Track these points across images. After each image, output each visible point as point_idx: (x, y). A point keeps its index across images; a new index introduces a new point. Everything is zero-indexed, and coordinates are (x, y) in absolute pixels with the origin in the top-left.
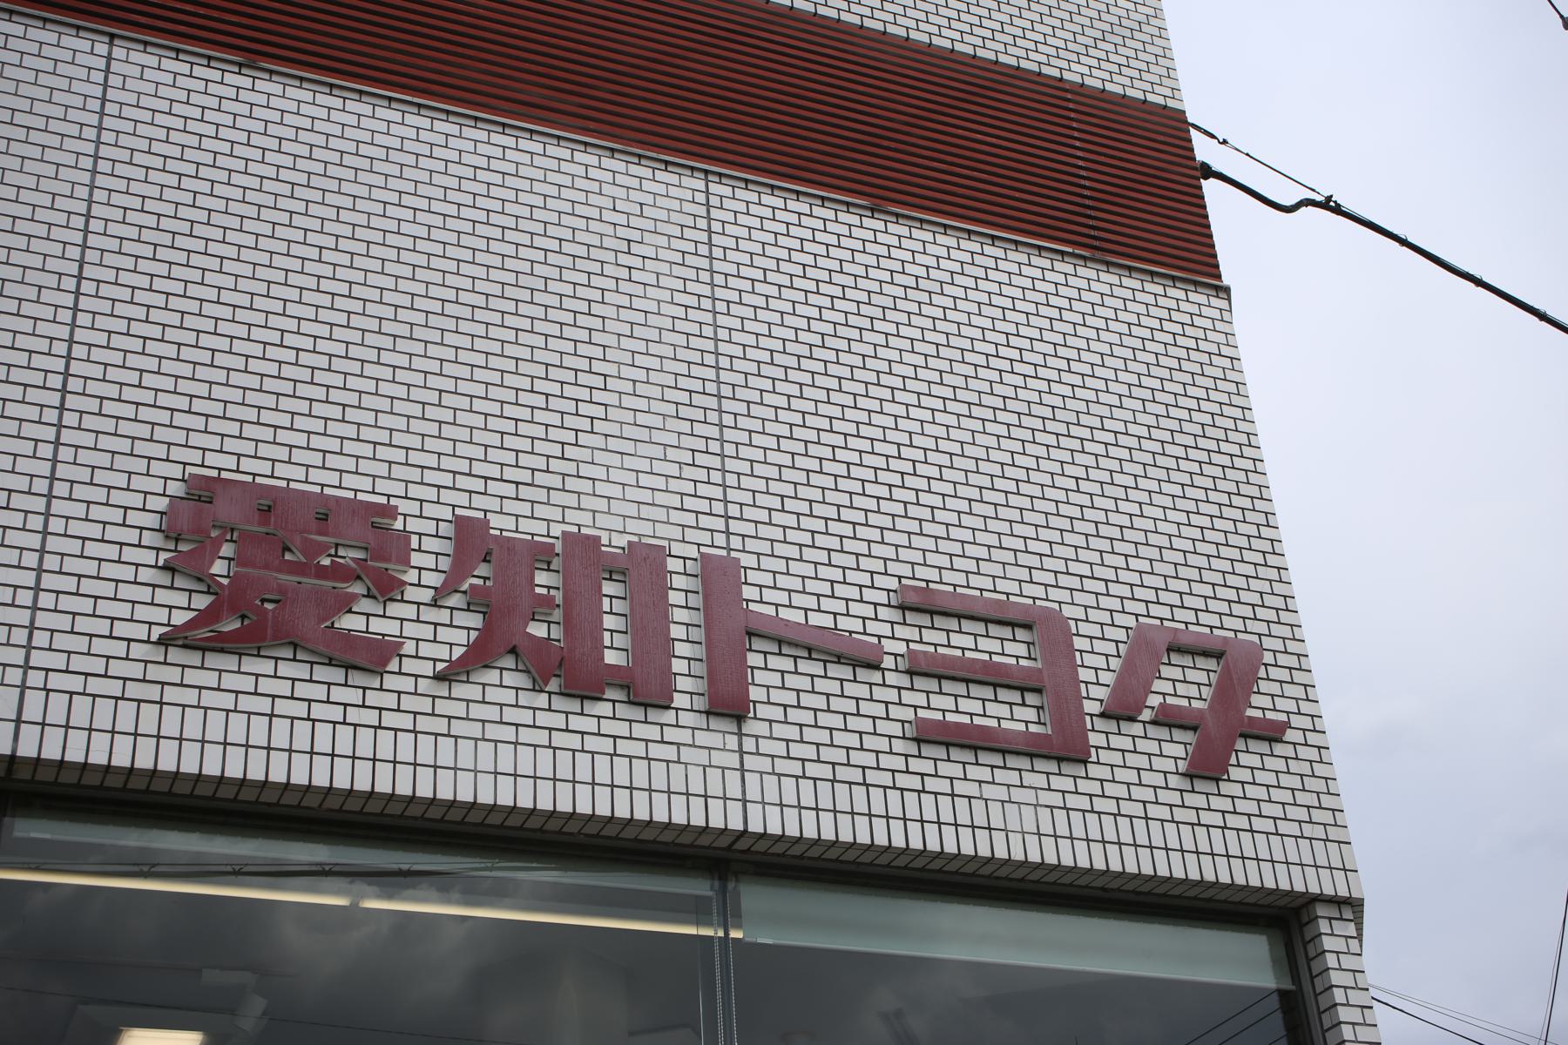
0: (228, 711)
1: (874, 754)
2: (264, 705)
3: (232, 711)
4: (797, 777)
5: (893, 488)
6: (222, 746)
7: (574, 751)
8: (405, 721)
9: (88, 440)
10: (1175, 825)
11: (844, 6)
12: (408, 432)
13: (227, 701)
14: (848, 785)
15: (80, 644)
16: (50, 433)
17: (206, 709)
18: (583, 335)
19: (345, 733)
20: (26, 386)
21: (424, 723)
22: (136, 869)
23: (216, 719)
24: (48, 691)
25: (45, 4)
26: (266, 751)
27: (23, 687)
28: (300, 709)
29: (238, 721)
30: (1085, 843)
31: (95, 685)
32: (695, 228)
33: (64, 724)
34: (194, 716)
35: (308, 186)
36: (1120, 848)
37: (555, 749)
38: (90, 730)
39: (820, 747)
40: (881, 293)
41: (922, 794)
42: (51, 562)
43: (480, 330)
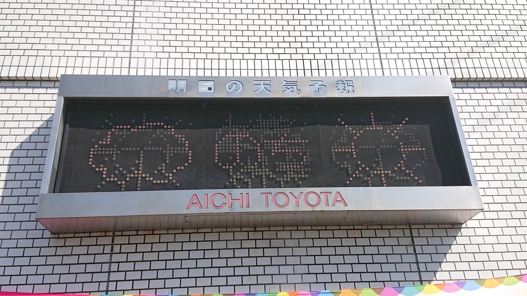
1: (444, 54)
3: (115, 57)
4: (446, 58)
5: (499, 42)
8: (264, 57)
9: (123, 19)
10: (423, 58)
11: (126, 3)
12: (329, 31)
13: (114, 54)
16: (131, 20)
17: (233, 59)
18: (425, 33)
20: (121, 17)
21: (185, 56)
22: (330, 212)
24: (268, 60)
26: (203, 70)
28: (191, 56)
29: (293, 63)
32: (485, 35)
33: (240, 69)
34: (230, 62)
37: (423, 59)
38: (204, 69)
40: (463, 35)
41: (410, 59)
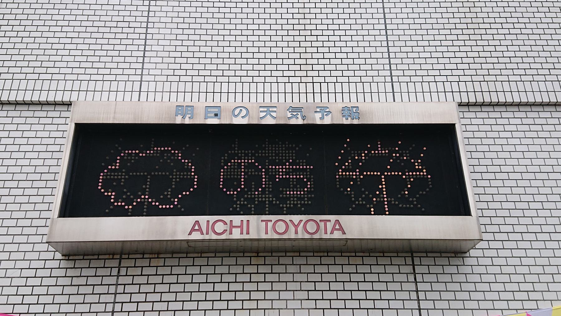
0: (299, 83)
2: (189, 79)
6: (250, 92)
7: (337, 82)
13: (298, 80)
14: (497, 58)
15: (196, 67)
19: (253, 86)
23: (295, 86)
25: (459, 155)
27: (392, 82)
30: (541, 91)
31: (207, 79)
34: (239, 85)
35: (404, 309)
36: (540, 90)
37: (435, 82)
39: (502, 24)
41: (545, 80)
42: (144, 25)
43: (472, 66)
